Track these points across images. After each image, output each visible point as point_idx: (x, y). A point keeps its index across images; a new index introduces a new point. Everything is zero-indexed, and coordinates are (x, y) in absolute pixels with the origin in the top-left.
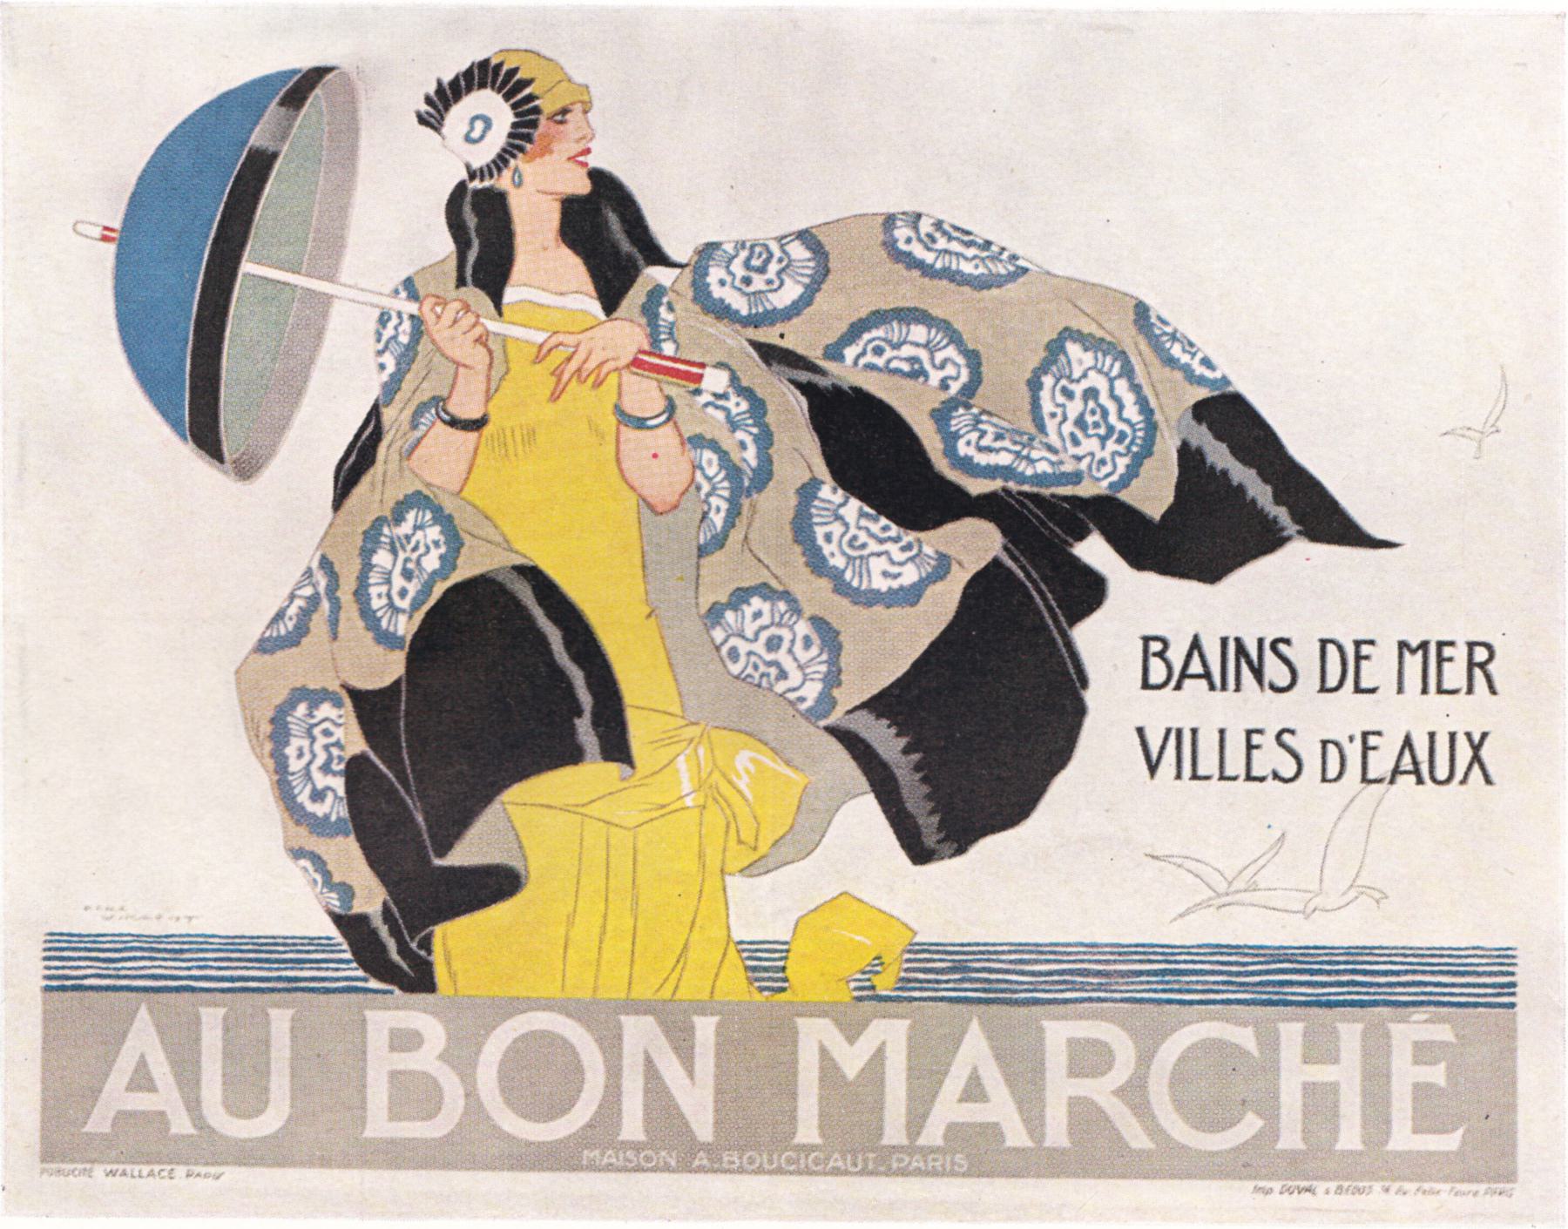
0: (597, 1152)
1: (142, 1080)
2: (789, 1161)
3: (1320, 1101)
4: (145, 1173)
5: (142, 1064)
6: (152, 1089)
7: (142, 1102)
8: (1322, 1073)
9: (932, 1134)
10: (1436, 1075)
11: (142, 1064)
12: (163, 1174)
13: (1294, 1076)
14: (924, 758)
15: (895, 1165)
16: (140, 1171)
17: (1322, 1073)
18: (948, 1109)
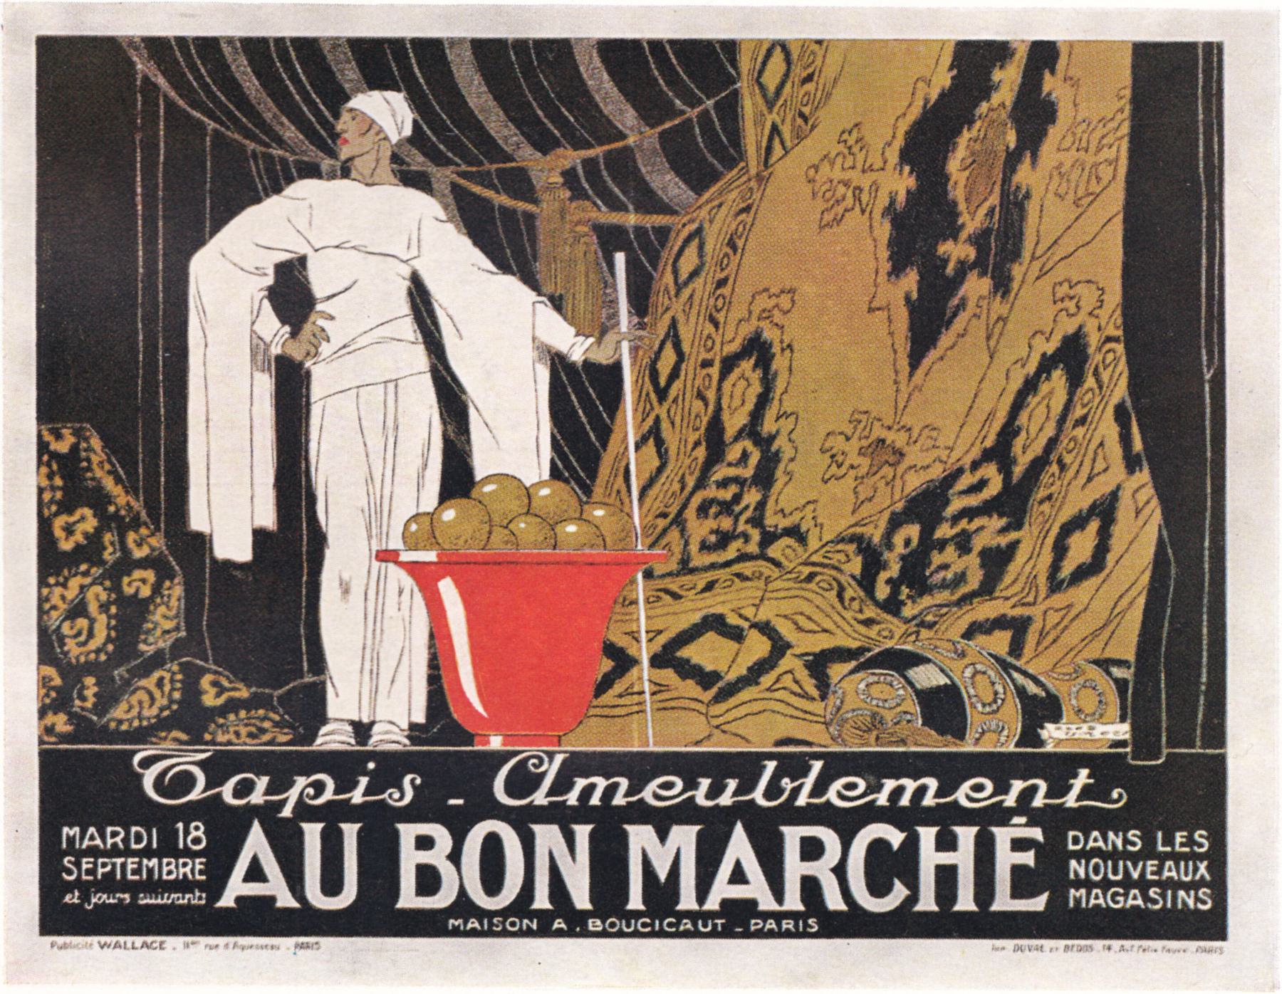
0: (460, 921)
1: (255, 874)
2: (644, 925)
3: (946, 876)
4: (129, 945)
5: (738, 864)
6: (745, 881)
7: (738, 892)
8: (946, 858)
9: (712, 904)
10: (1028, 858)
11: (738, 864)
12: (154, 945)
13: (930, 858)
14: (86, 545)
15: (753, 928)
16: (133, 943)
17: (946, 858)
18: (722, 890)
